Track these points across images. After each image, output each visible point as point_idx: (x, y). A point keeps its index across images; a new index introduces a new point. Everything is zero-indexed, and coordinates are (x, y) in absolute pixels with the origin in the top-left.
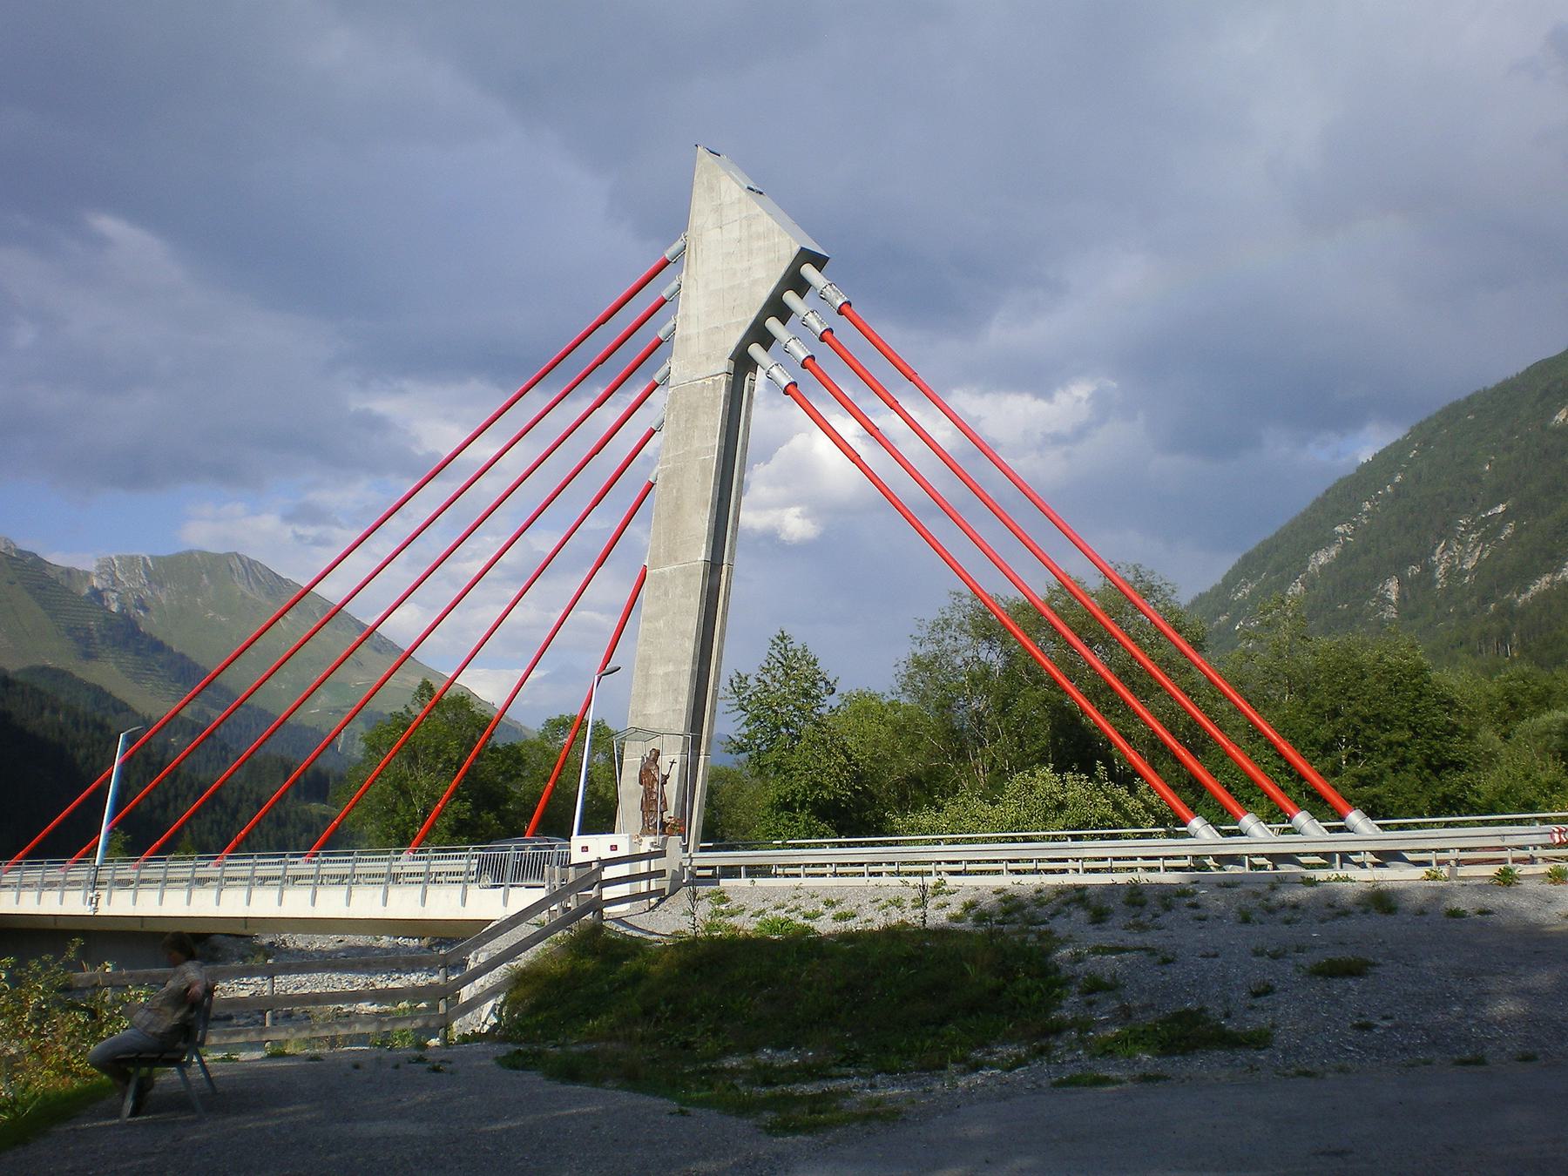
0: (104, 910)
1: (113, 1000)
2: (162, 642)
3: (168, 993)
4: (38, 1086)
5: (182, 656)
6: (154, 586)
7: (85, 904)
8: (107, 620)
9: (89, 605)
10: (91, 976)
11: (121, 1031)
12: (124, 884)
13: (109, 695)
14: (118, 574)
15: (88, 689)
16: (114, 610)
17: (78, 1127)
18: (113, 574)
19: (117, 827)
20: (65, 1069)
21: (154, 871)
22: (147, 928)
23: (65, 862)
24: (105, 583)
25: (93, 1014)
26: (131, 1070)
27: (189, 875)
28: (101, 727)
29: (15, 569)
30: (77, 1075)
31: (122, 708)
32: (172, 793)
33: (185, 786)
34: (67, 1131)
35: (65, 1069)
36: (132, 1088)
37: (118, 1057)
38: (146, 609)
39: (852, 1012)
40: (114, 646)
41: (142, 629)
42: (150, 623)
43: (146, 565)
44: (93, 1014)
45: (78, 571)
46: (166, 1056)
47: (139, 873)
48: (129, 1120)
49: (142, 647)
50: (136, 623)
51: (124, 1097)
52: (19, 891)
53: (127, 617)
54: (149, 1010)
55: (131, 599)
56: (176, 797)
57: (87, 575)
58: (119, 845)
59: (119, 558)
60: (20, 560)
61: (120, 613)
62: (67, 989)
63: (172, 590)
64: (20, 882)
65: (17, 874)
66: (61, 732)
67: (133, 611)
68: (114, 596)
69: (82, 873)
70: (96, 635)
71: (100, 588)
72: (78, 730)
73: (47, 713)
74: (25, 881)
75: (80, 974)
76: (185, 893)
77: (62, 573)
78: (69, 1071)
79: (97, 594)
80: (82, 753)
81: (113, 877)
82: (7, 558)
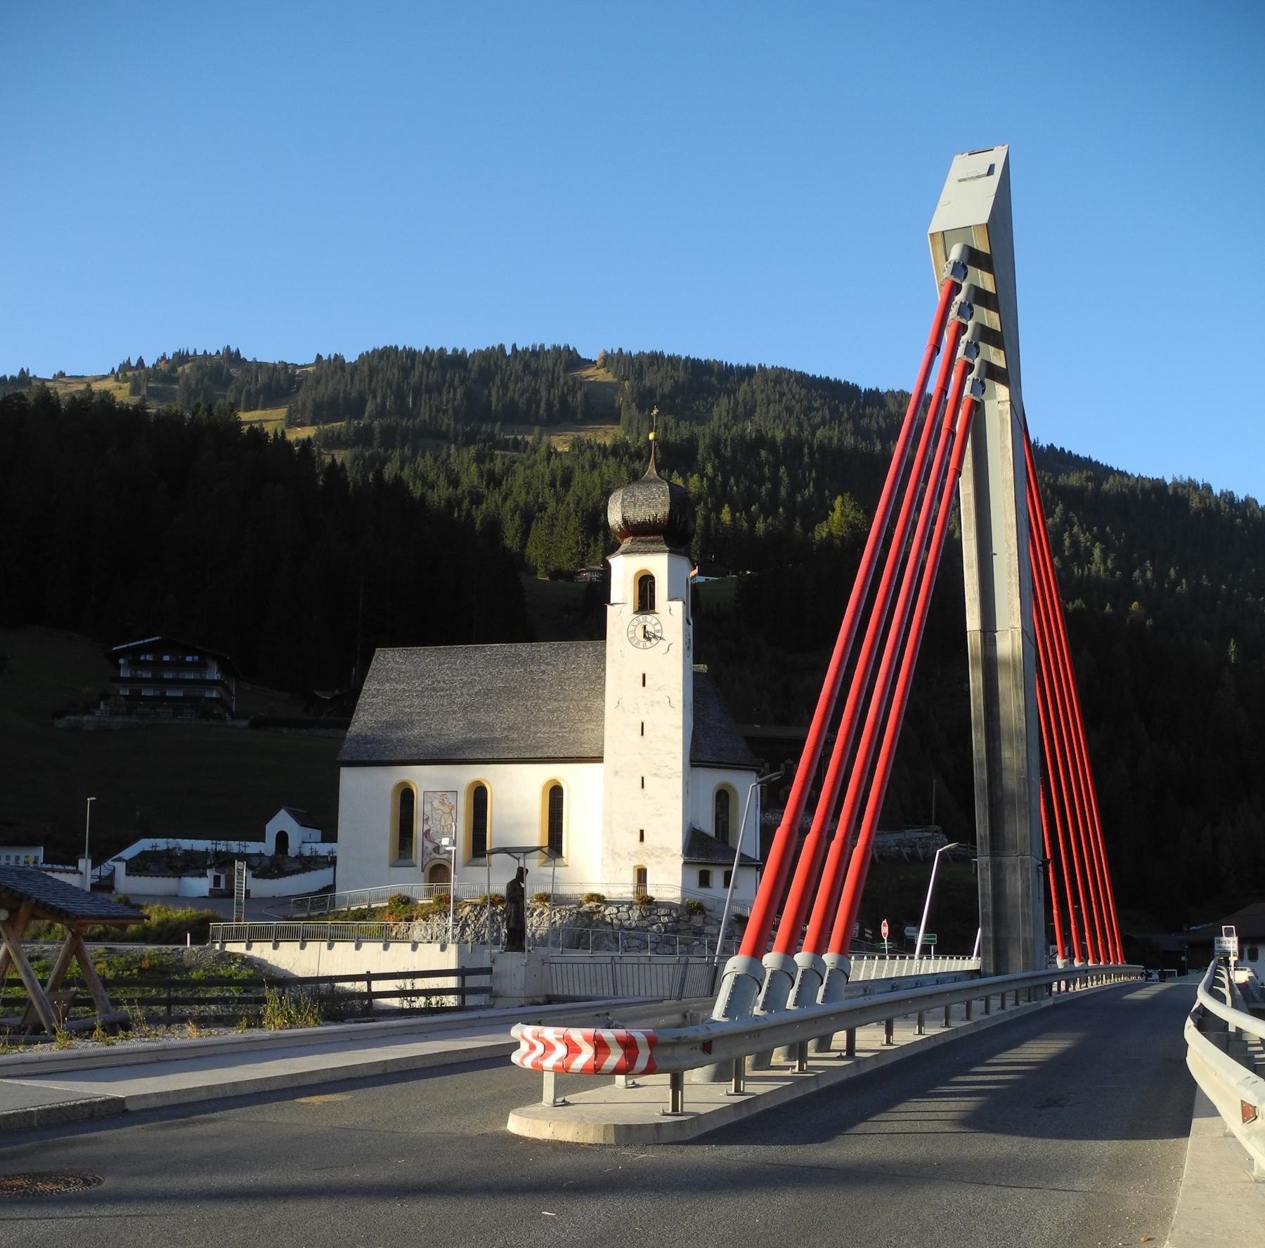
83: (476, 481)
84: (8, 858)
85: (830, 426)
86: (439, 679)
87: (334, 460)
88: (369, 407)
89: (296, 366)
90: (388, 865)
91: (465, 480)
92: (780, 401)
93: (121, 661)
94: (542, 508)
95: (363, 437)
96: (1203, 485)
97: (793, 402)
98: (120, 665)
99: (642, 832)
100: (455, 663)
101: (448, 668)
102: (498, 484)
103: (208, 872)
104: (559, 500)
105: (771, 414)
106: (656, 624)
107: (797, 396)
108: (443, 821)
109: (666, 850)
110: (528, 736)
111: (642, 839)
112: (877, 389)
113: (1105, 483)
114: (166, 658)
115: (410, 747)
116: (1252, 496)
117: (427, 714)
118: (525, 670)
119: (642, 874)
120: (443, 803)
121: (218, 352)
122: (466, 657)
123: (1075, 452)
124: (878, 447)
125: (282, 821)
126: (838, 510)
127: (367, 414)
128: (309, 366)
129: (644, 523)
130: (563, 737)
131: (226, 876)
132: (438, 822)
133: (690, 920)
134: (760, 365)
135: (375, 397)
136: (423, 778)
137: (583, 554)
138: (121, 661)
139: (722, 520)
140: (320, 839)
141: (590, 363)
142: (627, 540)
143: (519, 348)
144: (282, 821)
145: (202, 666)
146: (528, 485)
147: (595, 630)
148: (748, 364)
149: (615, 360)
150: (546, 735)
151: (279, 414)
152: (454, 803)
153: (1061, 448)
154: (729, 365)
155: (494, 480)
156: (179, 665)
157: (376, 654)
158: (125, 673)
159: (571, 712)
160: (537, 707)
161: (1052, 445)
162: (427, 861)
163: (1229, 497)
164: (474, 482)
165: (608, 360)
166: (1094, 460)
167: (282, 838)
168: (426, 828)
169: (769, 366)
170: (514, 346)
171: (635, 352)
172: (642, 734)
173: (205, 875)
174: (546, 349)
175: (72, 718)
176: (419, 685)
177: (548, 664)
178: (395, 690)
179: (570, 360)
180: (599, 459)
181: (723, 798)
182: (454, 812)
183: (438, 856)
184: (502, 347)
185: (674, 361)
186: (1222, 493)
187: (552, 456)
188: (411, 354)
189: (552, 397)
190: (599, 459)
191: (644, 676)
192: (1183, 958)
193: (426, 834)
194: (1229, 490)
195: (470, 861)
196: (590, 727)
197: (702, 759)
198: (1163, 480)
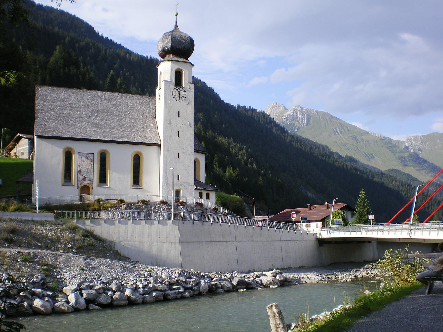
0: (413, 237)
1: (420, 262)
2: (426, 160)
3: (439, 260)
4: (399, 285)
5: (432, 164)
6: (423, 144)
7: (408, 235)
8: (410, 154)
9: (405, 151)
10: (413, 255)
11: (422, 272)
12: (418, 229)
13: (411, 176)
14: (413, 141)
15: (405, 175)
16: (412, 152)
17: (413, 296)
18: (411, 141)
19: (417, 213)
20: (406, 281)
21: (427, 226)
22: (425, 242)
23: (402, 223)
24: (409, 144)
25: (414, 266)
26: (428, 281)
27: (438, 227)
28: (409, 185)
29: (383, 142)
30: (409, 282)
31: (415, 180)
32: (430, 204)
33: (434, 201)
34: (410, 297)
35: (406, 281)
36: (428, 286)
37: (425, 278)
38: (421, 151)
39: (90, 245)
40: (412, 162)
41: (420, 157)
42: (422, 155)
43: (420, 138)
44: (414, 266)
45: (401, 141)
46: (439, 278)
47: (423, 226)
48: (427, 295)
49: (421, 162)
50: (419, 155)
51: (426, 289)
52: (401, 231)
53: (416, 154)
54: (434, 265)
55: (417, 148)
56: (432, 204)
57: (404, 142)
58: (416, 219)
59: (413, 136)
60: (385, 140)
61: (414, 153)
62: (406, 258)
63: (429, 145)
64: (378, 229)
65: (388, 227)
66: (398, 187)
67: (417, 152)
68: (412, 148)
69: (406, 226)
70: (407, 159)
71: (408, 146)
72: (403, 187)
73: (394, 182)
74: (391, 229)
75: (410, 254)
76: (437, 232)
77: (397, 142)
78: (407, 281)
79: (407, 147)
80: (404, 193)
81: (416, 228)
82: (381, 139)
99: (178, 176)
100: (77, 96)
109: (189, 184)
111: (178, 179)
123: (116, 41)
126: (58, 50)
132: (85, 167)
136: (77, 147)
152: (92, 159)
159: (137, 124)
162: (80, 183)
166: (122, 45)
168: (79, 169)
176: (63, 104)
191: (179, 112)
193: (79, 172)
195: (99, 185)
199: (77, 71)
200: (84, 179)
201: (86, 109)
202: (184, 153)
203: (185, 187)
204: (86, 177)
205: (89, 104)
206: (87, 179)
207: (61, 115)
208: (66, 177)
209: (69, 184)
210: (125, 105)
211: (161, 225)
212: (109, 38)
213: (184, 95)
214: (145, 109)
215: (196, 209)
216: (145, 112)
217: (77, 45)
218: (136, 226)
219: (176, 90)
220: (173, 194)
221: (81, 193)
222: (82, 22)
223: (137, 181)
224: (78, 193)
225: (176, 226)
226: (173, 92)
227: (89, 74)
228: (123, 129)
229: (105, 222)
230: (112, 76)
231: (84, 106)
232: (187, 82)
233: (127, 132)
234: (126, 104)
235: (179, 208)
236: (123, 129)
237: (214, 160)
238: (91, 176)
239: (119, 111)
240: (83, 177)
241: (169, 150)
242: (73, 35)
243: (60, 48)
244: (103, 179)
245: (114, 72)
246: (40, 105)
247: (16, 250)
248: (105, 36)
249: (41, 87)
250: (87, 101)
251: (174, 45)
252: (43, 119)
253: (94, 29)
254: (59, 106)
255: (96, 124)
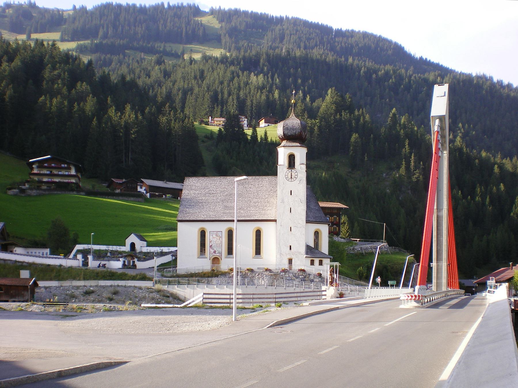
83: (159, 75)
84: (39, 253)
85: (319, 47)
86: (211, 189)
87: (104, 72)
88: (101, 33)
89: (63, 11)
90: (197, 257)
91: (153, 74)
92: (296, 34)
93: (34, 166)
94: (192, 90)
95: (97, 49)
96: (489, 77)
97: (302, 35)
98: (33, 168)
99: (290, 246)
101: (214, 185)
102: (169, 77)
103: (121, 259)
104: (200, 86)
105: (292, 40)
106: (295, 173)
107: (304, 32)
108: (217, 242)
109: (300, 253)
110: (247, 211)
111: (290, 249)
112: (341, 29)
113: (446, 77)
114: (53, 165)
115: (204, 215)
116: (511, 82)
117: (209, 203)
118: (243, 186)
119: (290, 261)
120: (217, 235)
121: (25, 3)
122: (220, 181)
123: (432, 60)
124: (343, 59)
125: (133, 238)
126: (329, 95)
127: (99, 36)
128: (69, 10)
129: (291, 135)
130: (260, 212)
131: (128, 261)
133: (309, 277)
134: (286, 16)
135: (103, 28)
136: (209, 227)
137: (212, 112)
138: (34, 166)
139: (275, 97)
140: (146, 246)
141: (204, 14)
142: (284, 141)
143: (171, 4)
144: (133, 238)
145: (69, 169)
146: (184, 78)
147: (274, 172)
148: (280, 16)
149: (217, 13)
150: (254, 212)
151: (55, 36)
153: (426, 58)
154: (271, 16)
155: (167, 74)
156: (61, 168)
157: (186, 179)
158: (35, 171)
160: (249, 201)
161: (421, 57)
162: (212, 256)
163: (500, 83)
164: (158, 75)
165: (213, 12)
167: (133, 245)
168: (211, 244)
169: (290, 17)
170: (169, 4)
171: (227, 9)
172: (291, 212)
173: (119, 260)
174: (184, 5)
175: (15, 190)
176: (204, 192)
177: (252, 185)
178: (195, 194)
179: (196, 11)
180: (215, 66)
181: (317, 234)
182: (221, 239)
183: (215, 254)
184: (163, 4)
185: (245, 13)
186: (497, 81)
187: (192, 62)
188: (119, 6)
189: (188, 29)
190: (215, 66)
191: (291, 191)
192: (474, 289)
194: (501, 79)
195: (227, 256)
196: (270, 209)
197: (310, 220)
198: (472, 74)
199: (350, 115)
200: (215, 252)
201: (221, 194)
202: (295, 226)
203: (296, 256)
204: (216, 250)
205: (225, 189)
206: (217, 252)
207: (200, 201)
208: (201, 251)
209: (203, 256)
210: (255, 187)
211: (228, 289)
212: (424, 58)
213: (296, 175)
214: (272, 189)
215: (298, 275)
216: (271, 191)
217: (374, 76)
218: (210, 289)
219: (288, 172)
220: (286, 262)
221: (213, 263)
222: (390, 42)
223: (258, 251)
224: (210, 263)
225: (191, 290)
226: (286, 174)
227: (364, 118)
228: (248, 209)
229: (207, 287)
230: (394, 115)
231: (221, 191)
232: (299, 164)
233: (251, 211)
234: (257, 186)
235: (281, 274)
236: (248, 209)
237: (514, 206)
238: (220, 250)
239: (249, 194)
240: (214, 251)
241: (282, 224)
242: (370, 64)
243: (331, 92)
244: (230, 251)
245: (396, 110)
246: (185, 195)
247: (103, 305)
248: (418, 56)
249: (189, 179)
250: (224, 187)
251: (286, 132)
252: (185, 206)
253: (405, 50)
254: (201, 194)
255: (226, 207)
